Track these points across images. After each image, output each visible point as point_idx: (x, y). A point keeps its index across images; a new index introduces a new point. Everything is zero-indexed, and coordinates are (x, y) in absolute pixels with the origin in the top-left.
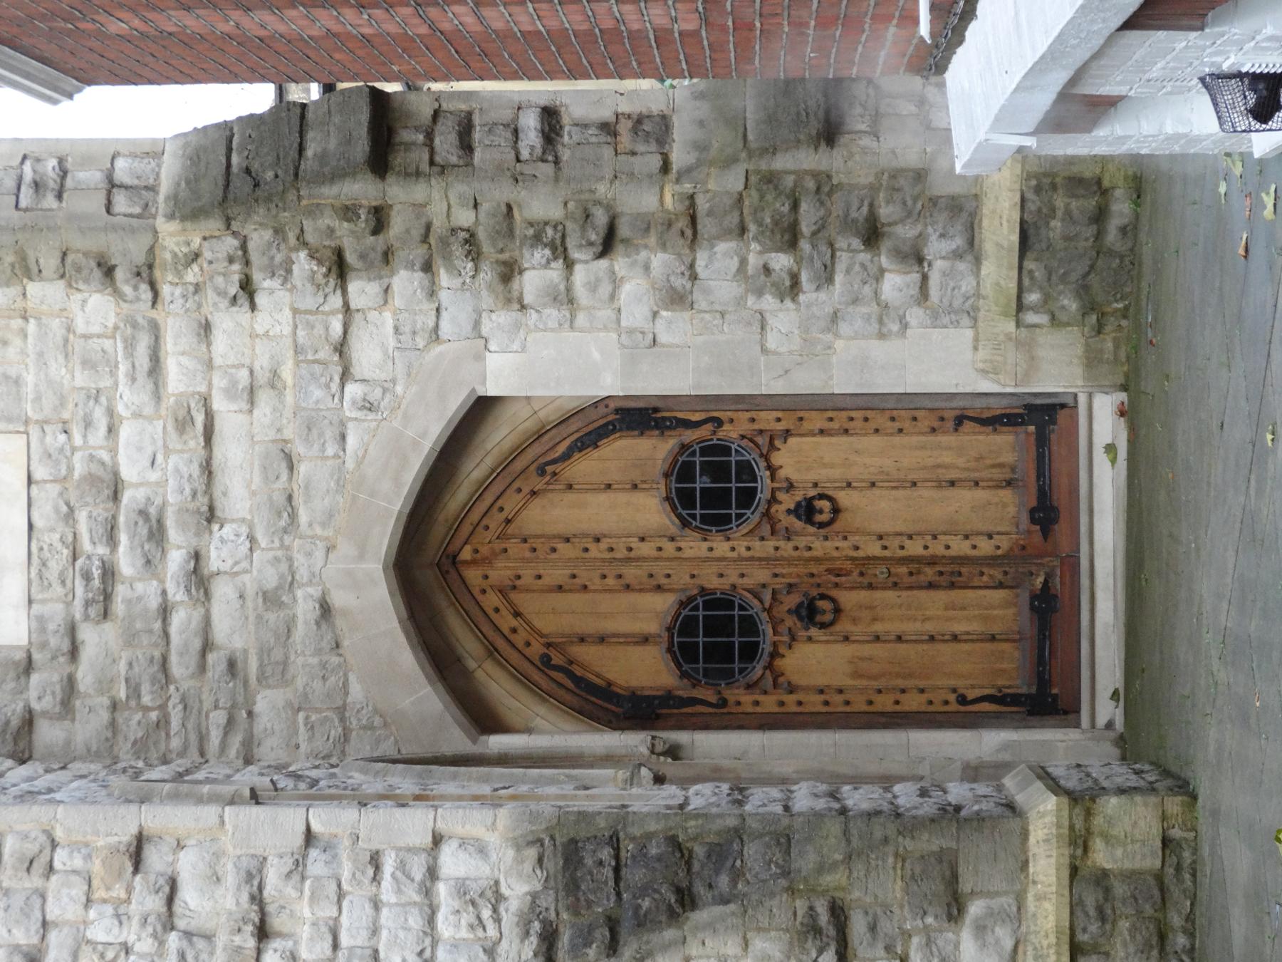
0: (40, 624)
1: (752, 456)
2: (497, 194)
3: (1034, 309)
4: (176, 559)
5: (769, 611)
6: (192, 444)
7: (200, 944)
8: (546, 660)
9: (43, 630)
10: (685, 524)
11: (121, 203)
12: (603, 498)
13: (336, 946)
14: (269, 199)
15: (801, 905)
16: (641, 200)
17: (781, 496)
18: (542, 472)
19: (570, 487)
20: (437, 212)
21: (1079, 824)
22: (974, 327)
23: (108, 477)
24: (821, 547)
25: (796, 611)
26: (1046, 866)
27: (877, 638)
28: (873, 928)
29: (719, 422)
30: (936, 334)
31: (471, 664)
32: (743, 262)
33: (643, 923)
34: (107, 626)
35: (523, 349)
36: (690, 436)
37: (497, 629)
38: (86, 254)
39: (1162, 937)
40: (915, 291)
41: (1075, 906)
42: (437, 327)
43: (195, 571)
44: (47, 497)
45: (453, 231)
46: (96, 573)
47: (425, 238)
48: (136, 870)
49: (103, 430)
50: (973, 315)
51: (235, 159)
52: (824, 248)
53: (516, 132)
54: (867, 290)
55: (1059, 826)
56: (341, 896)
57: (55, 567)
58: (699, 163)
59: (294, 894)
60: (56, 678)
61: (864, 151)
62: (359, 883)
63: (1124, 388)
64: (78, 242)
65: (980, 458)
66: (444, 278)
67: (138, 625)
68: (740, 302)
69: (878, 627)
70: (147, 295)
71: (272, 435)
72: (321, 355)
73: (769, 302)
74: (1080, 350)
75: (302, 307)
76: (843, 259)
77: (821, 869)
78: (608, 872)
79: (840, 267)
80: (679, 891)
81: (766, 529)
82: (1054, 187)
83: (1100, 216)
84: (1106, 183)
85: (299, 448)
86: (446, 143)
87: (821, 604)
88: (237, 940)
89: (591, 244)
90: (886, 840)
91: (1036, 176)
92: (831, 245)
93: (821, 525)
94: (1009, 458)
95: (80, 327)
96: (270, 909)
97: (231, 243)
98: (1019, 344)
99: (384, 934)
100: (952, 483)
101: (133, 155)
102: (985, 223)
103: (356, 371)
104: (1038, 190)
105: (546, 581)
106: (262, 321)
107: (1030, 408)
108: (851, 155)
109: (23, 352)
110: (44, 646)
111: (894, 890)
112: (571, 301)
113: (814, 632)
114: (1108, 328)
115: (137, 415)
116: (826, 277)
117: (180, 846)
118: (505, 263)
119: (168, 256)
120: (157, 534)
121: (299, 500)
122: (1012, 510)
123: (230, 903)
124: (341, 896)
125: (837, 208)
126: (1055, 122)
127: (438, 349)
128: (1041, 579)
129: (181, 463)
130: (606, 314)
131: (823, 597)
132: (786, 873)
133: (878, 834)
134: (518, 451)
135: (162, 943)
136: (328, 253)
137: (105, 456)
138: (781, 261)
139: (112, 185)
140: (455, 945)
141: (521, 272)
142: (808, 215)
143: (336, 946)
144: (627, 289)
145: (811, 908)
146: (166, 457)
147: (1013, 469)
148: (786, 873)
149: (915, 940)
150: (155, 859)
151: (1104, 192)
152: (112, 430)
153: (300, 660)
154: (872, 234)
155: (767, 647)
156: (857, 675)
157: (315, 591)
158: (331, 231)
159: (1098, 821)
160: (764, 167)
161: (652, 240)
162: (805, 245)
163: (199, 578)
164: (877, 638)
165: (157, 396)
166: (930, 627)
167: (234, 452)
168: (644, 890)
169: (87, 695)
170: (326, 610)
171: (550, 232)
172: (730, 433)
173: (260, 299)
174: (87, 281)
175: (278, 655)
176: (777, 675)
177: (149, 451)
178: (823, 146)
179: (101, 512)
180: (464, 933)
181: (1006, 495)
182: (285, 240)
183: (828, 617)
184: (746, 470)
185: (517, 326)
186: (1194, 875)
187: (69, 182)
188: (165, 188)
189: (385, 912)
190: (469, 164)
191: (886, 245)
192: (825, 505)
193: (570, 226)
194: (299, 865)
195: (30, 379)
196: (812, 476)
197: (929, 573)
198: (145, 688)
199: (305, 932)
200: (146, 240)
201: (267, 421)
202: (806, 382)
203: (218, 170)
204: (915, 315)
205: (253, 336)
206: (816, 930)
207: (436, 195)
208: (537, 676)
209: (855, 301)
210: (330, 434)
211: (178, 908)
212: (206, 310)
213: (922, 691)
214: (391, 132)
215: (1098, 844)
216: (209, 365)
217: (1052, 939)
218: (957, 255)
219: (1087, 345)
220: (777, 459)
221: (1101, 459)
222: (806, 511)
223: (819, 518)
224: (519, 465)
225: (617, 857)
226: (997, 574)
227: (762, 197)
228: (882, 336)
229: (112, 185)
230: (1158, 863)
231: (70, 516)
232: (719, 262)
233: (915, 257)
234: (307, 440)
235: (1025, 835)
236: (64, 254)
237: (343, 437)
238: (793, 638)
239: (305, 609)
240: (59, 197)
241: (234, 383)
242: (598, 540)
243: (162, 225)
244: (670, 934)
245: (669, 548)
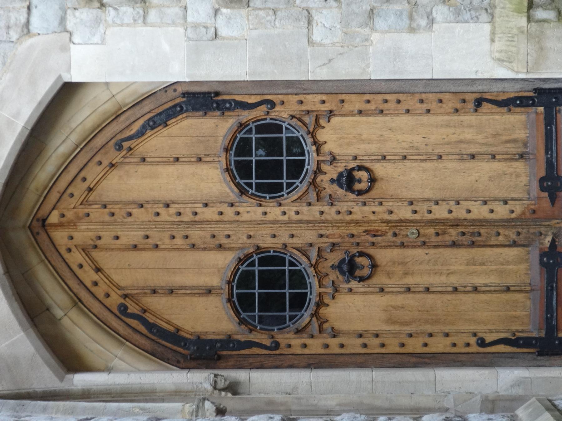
1: (301, 133)
8: (123, 309)
10: (243, 192)
17: (325, 167)
18: (119, 147)
19: (144, 160)
22: (492, 21)
24: (360, 212)
25: (339, 267)
29: (272, 104)
30: (459, 28)
31: (59, 313)
35: (103, 41)
36: (246, 116)
37: (81, 282)
42: (28, 22)
65: (496, 135)
69: (410, 281)
81: (312, 196)
87: (360, 260)
93: (360, 193)
94: (521, 134)
98: (529, 36)
107: (539, 91)
113: (354, 284)
122: (524, 179)
127: (29, 42)
128: (549, 239)
147: (525, 145)
155: (313, 298)
156: (390, 321)
166: (454, 280)
172: (281, 113)
181: (519, 166)
183: (366, 272)
185: (98, 21)
192: (363, 175)
196: (352, 150)
197: (453, 234)
202: (346, 69)
213: (447, 335)
220: (322, 136)
222: (347, 180)
224: (99, 141)
228: (412, 30)
238: (336, 290)
242: (168, 206)
245: (229, 212)
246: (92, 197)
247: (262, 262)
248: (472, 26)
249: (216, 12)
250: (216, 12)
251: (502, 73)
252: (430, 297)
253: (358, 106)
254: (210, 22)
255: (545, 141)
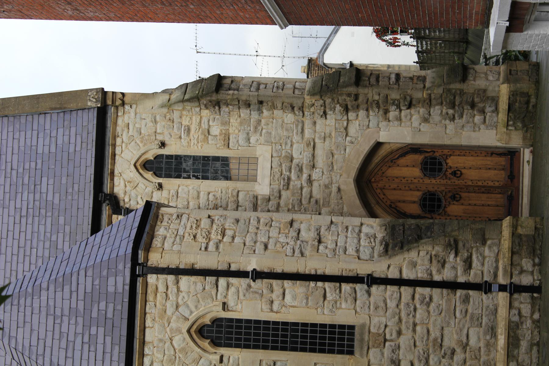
0: (272, 190)
1: (442, 160)
2: (385, 92)
3: (511, 126)
4: (305, 176)
5: (444, 197)
6: (310, 150)
7: (305, 243)
8: (391, 206)
9: (273, 191)
10: (425, 175)
11: (297, 92)
12: (406, 168)
13: (336, 245)
14: (331, 91)
15: (447, 239)
16: (418, 95)
17: (448, 170)
18: (392, 162)
19: (398, 165)
20: (370, 96)
21: (515, 223)
22: (496, 130)
23: (290, 156)
24: (457, 182)
25: (451, 197)
26: (506, 232)
27: (470, 205)
28: (464, 246)
29: (434, 152)
30: (487, 131)
31: (373, 205)
32: (442, 111)
33: (409, 242)
34: (288, 191)
35: (389, 131)
36: (427, 155)
37: (379, 198)
38: (288, 103)
39: (534, 251)
40: (482, 120)
41: (513, 242)
42: (369, 125)
43: (309, 179)
44: (276, 161)
45: (374, 101)
46: (286, 179)
47: (367, 103)
48: (291, 227)
49: (290, 145)
50: (496, 127)
51: (324, 83)
52: (461, 108)
53: (389, 78)
54: (471, 120)
55: (510, 223)
56: (338, 235)
57: (276, 178)
58: (432, 86)
59: (327, 234)
60: (275, 203)
61: (472, 84)
62: (343, 232)
63: (532, 146)
64: (287, 101)
65: (497, 163)
66: (371, 113)
67: (295, 191)
68: (441, 122)
69: (470, 202)
70: (302, 114)
71: (329, 148)
72: (341, 130)
73: (447, 122)
74: (522, 136)
75: (337, 118)
76: (466, 111)
77: (452, 231)
78: (402, 231)
79: (465, 114)
80: (418, 236)
81: (444, 177)
82: (517, 94)
83: (528, 102)
84: (530, 94)
85: (335, 152)
86: (373, 80)
87: (456, 196)
88: (314, 243)
89: (406, 105)
90: (468, 225)
91: (513, 91)
92: (463, 108)
93: (458, 177)
94: (503, 163)
95: (286, 121)
96: (322, 237)
97: (322, 102)
98: (507, 134)
99: (348, 243)
100: (490, 169)
101: (300, 82)
102: (500, 103)
103: (349, 134)
104: (513, 95)
105: (392, 187)
106: (328, 122)
107: (509, 152)
108: (469, 85)
109: (272, 127)
110: (273, 195)
111: (470, 237)
112: (401, 120)
113: (455, 202)
114: (529, 131)
115: (298, 142)
116: (461, 116)
117: (301, 223)
118: (385, 109)
119: (307, 104)
120: (301, 170)
121: (334, 164)
122: (504, 176)
123: (312, 235)
124: (338, 235)
125: (465, 99)
126: (519, 60)
127: (368, 130)
128: (510, 192)
129: (307, 154)
130: (409, 123)
131: (457, 194)
132: (444, 232)
133: (466, 223)
134: (386, 156)
135: (296, 243)
136: (344, 105)
137: (290, 151)
138: (451, 112)
139: (295, 88)
140: (365, 247)
141: (389, 112)
142: (458, 100)
143: (336, 245)
144: (414, 117)
145: (449, 240)
146: (304, 153)
147: (504, 166)
148: (444, 232)
149: (474, 249)
150: (296, 225)
151: (529, 96)
152: (291, 146)
153: (333, 201)
154: (473, 106)
155: (443, 205)
156: (464, 213)
157: (337, 185)
158: (345, 100)
159: (519, 222)
160: (448, 87)
161: (420, 105)
162: (457, 108)
163: (310, 181)
164: (470, 205)
165: (303, 138)
166: (483, 202)
167: (320, 153)
168: (410, 236)
169: (282, 207)
170: (339, 190)
171: (396, 102)
172: (437, 154)
173: (328, 116)
174: (288, 110)
175: (327, 200)
176: (445, 212)
177: (300, 151)
178: (462, 83)
179: (288, 164)
180: (367, 244)
181: (502, 172)
182: (334, 101)
183: (458, 199)
184: (440, 164)
185: (388, 125)
186: (542, 237)
187: (285, 87)
188: (307, 89)
189: (348, 239)
190: (378, 85)
191: (476, 109)
192: (459, 172)
193: (401, 100)
194: (329, 228)
195: (273, 133)
196: (456, 166)
197: (483, 189)
198: (296, 206)
199: (330, 242)
200: (302, 100)
201: (328, 145)
202: (455, 141)
203: (319, 85)
204: (482, 127)
205: (326, 125)
206: (450, 245)
207: (370, 92)
208: (388, 209)
209: (468, 122)
210: (342, 149)
211: (300, 236)
212: (315, 119)
213: (480, 217)
214: (360, 77)
215: (519, 228)
216: (315, 131)
217: (507, 250)
218: (493, 112)
219: (523, 135)
220: (448, 161)
221: (526, 164)
222: (454, 173)
223: (457, 175)
224: (386, 160)
225: (404, 228)
226: (499, 190)
227: (447, 95)
228: (474, 131)
229: (295, 88)
230: (534, 233)
231: (281, 165)
232: (436, 111)
233: (483, 112)
234: (337, 150)
235: (502, 225)
236: (283, 103)
237: (345, 150)
238: (450, 204)
239: (334, 189)
240: (282, 90)
241: (321, 136)
242: (404, 178)
243: (306, 96)
244: (415, 245)
245: (421, 181)
246: (384, 175)
247: (430, 195)
248: (491, 131)
249: (420, 124)
250: (420, 124)
251: (499, 144)
252: (476, 207)
253: (458, 153)
254: (418, 127)
255: (266, 270)
